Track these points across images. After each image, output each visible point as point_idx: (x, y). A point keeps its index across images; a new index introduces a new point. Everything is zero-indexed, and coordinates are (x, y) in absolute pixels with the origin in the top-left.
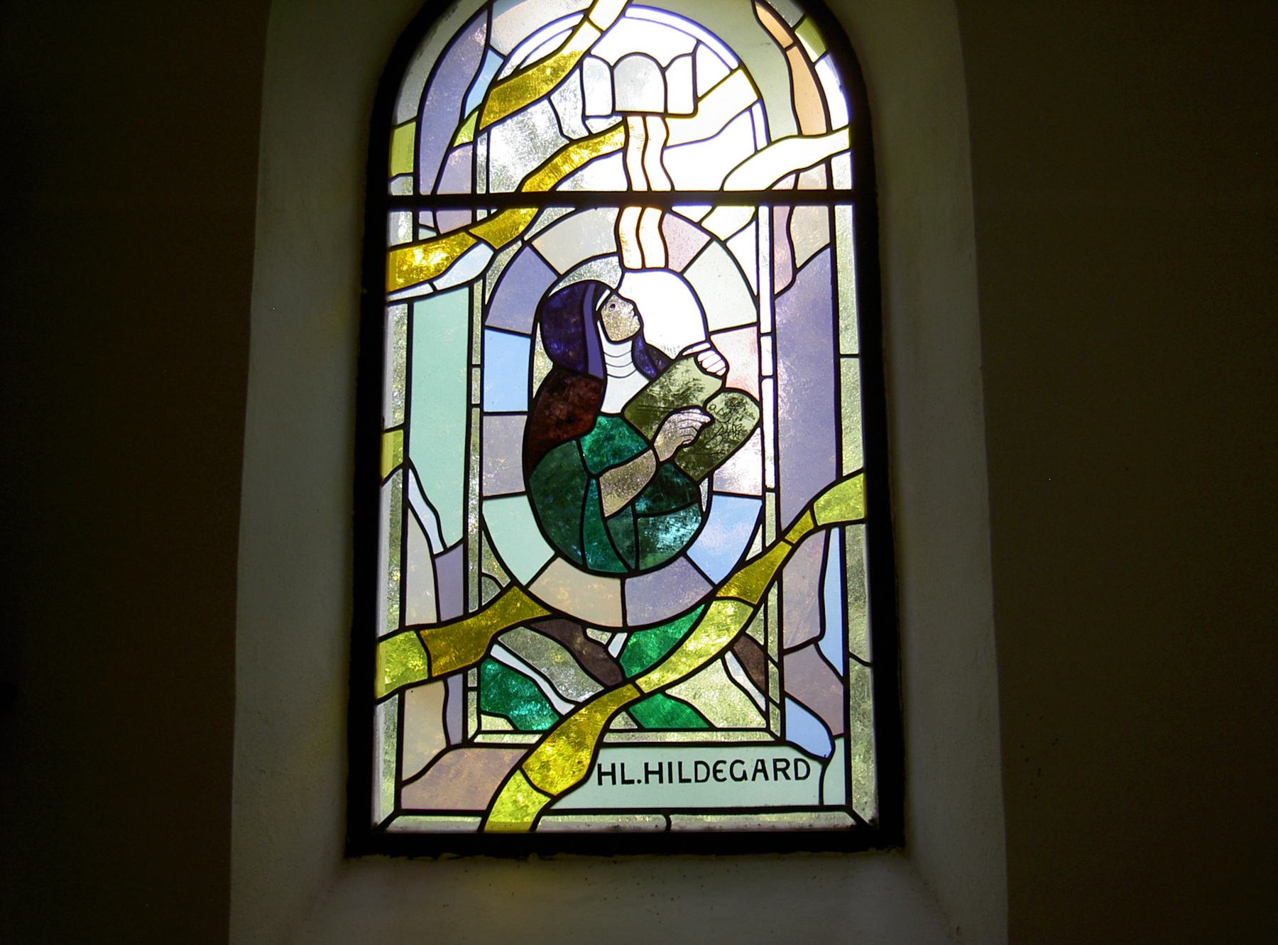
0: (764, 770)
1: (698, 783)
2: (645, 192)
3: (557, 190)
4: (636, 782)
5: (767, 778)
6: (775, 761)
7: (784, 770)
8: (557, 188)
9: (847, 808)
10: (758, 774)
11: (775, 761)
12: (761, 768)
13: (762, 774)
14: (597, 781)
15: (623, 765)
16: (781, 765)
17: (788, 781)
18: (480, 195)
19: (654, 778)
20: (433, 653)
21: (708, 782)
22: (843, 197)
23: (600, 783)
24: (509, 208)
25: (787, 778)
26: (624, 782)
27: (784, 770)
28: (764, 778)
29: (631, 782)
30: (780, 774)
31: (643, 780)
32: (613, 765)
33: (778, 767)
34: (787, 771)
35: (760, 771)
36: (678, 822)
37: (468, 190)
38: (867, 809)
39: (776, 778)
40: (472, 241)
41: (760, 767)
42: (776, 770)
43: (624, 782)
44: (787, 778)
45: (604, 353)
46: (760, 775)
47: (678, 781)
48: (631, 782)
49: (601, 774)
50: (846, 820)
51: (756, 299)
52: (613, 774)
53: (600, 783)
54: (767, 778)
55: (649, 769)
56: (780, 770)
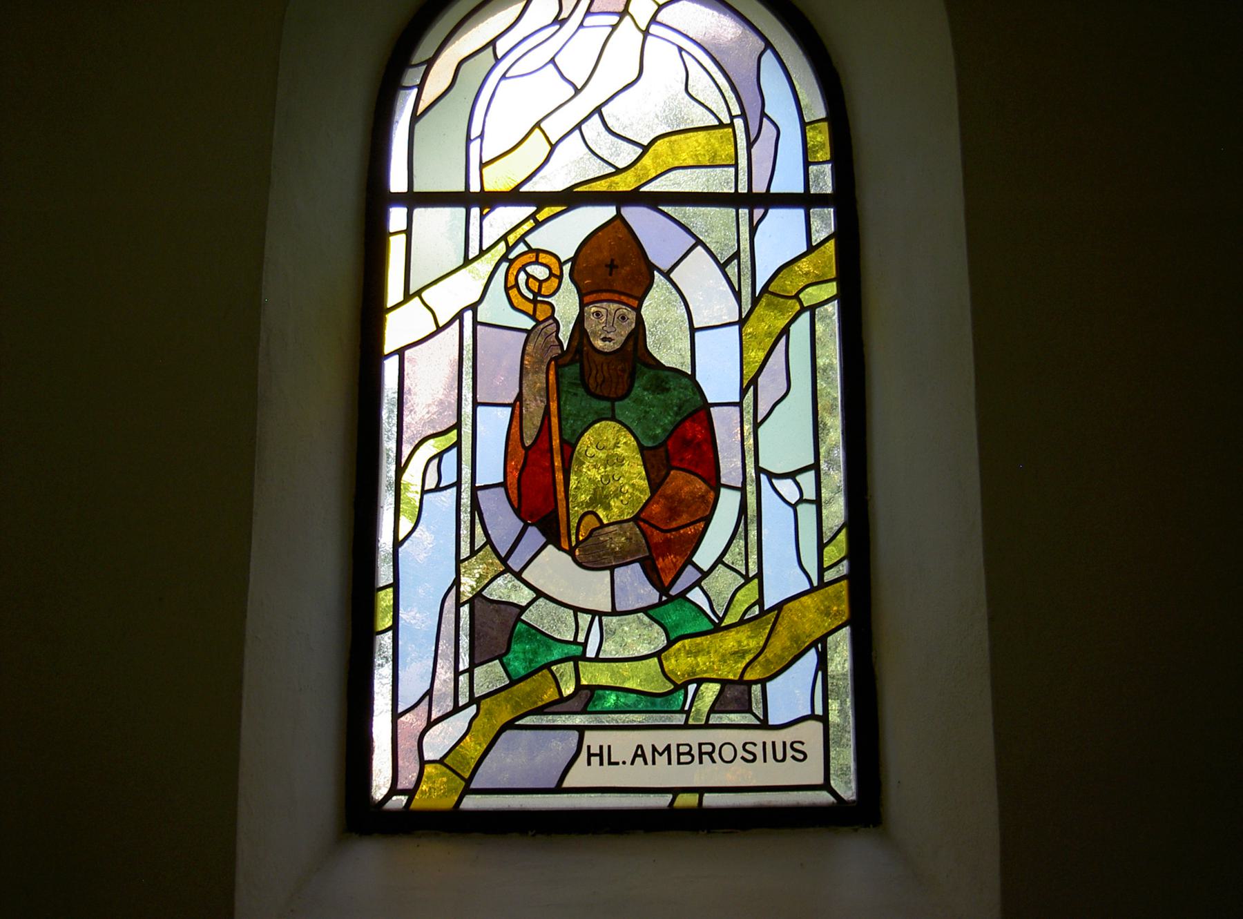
0: (643, 756)
1: (610, 766)
2: (405, 193)
3: (521, 190)
4: (621, 763)
5: (646, 763)
6: (700, 745)
7: (710, 754)
8: (520, 188)
9: (826, 786)
10: (637, 759)
11: (678, 746)
12: (639, 753)
13: (641, 759)
14: (586, 762)
15: (609, 747)
16: (706, 748)
17: (714, 764)
18: (741, 193)
19: (639, 760)
20: (668, 626)
21: (806, 751)
22: (399, 199)
23: (589, 764)
24: (548, 206)
25: (714, 761)
26: (610, 763)
27: (710, 754)
28: (643, 763)
29: (617, 763)
30: (705, 757)
31: (629, 761)
32: (601, 747)
33: (703, 751)
34: (713, 755)
35: (639, 756)
36: (710, 800)
37: (462, 189)
38: (847, 789)
39: (701, 762)
40: (817, 238)
41: (639, 752)
42: (701, 754)
43: (610, 763)
44: (714, 761)
45: (559, 345)
46: (639, 760)
47: (676, 763)
48: (617, 763)
49: (590, 755)
50: (824, 797)
51: (738, 295)
52: (601, 755)
53: (589, 764)
54: (646, 763)
55: (592, 752)
56: (706, 753)
